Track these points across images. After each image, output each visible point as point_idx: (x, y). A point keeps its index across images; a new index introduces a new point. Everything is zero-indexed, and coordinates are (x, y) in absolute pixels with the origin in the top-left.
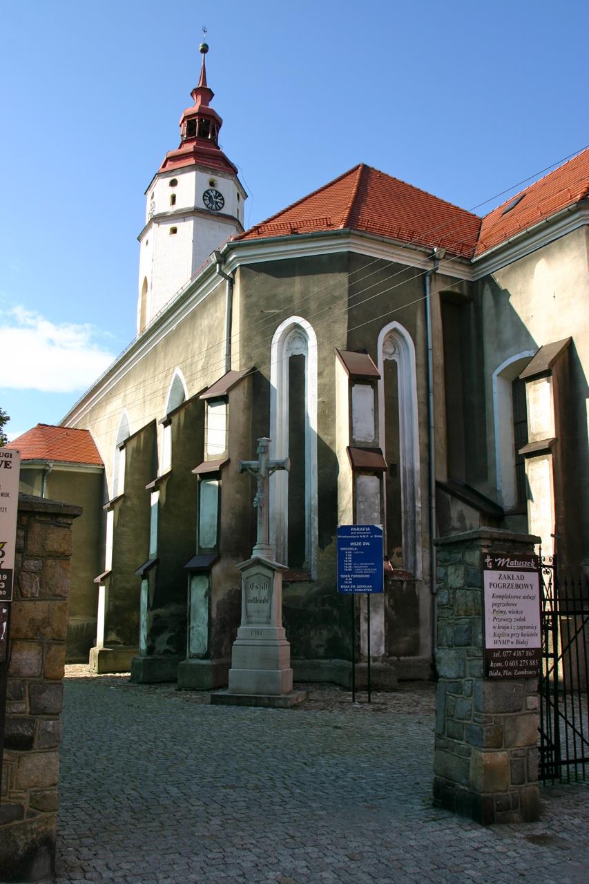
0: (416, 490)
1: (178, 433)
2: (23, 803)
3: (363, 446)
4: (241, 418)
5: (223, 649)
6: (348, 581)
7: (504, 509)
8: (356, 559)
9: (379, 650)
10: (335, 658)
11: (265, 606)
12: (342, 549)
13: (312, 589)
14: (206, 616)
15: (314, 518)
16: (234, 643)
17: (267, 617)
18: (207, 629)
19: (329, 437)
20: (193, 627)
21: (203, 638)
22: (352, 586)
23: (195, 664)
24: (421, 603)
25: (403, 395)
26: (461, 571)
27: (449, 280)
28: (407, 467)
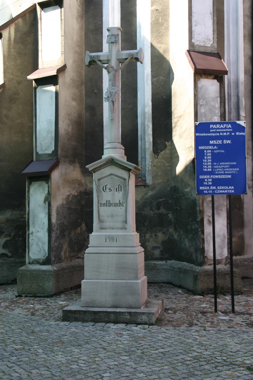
0: (240, 100)
1: (9, 48)
3: (202, 50)
4: (75, 25)
5: (62, 253)
6: (207, 182)
8: (216, 158)
9: (222, 252)
10: (170, 260)
11: (120, 210)
12: (200, 148)
13: (146, 194)
14: (46, 221)
15: (148, 125)
16: (86, 251)
17: (123, 222)
18: (47, 234)
19: (162, 46)
20: (32, 233)
21: (43, 244)
22: (211, 188)
23: (35, 270)
24: (245, 206)
25: (229, 8)
28: (232, 79)
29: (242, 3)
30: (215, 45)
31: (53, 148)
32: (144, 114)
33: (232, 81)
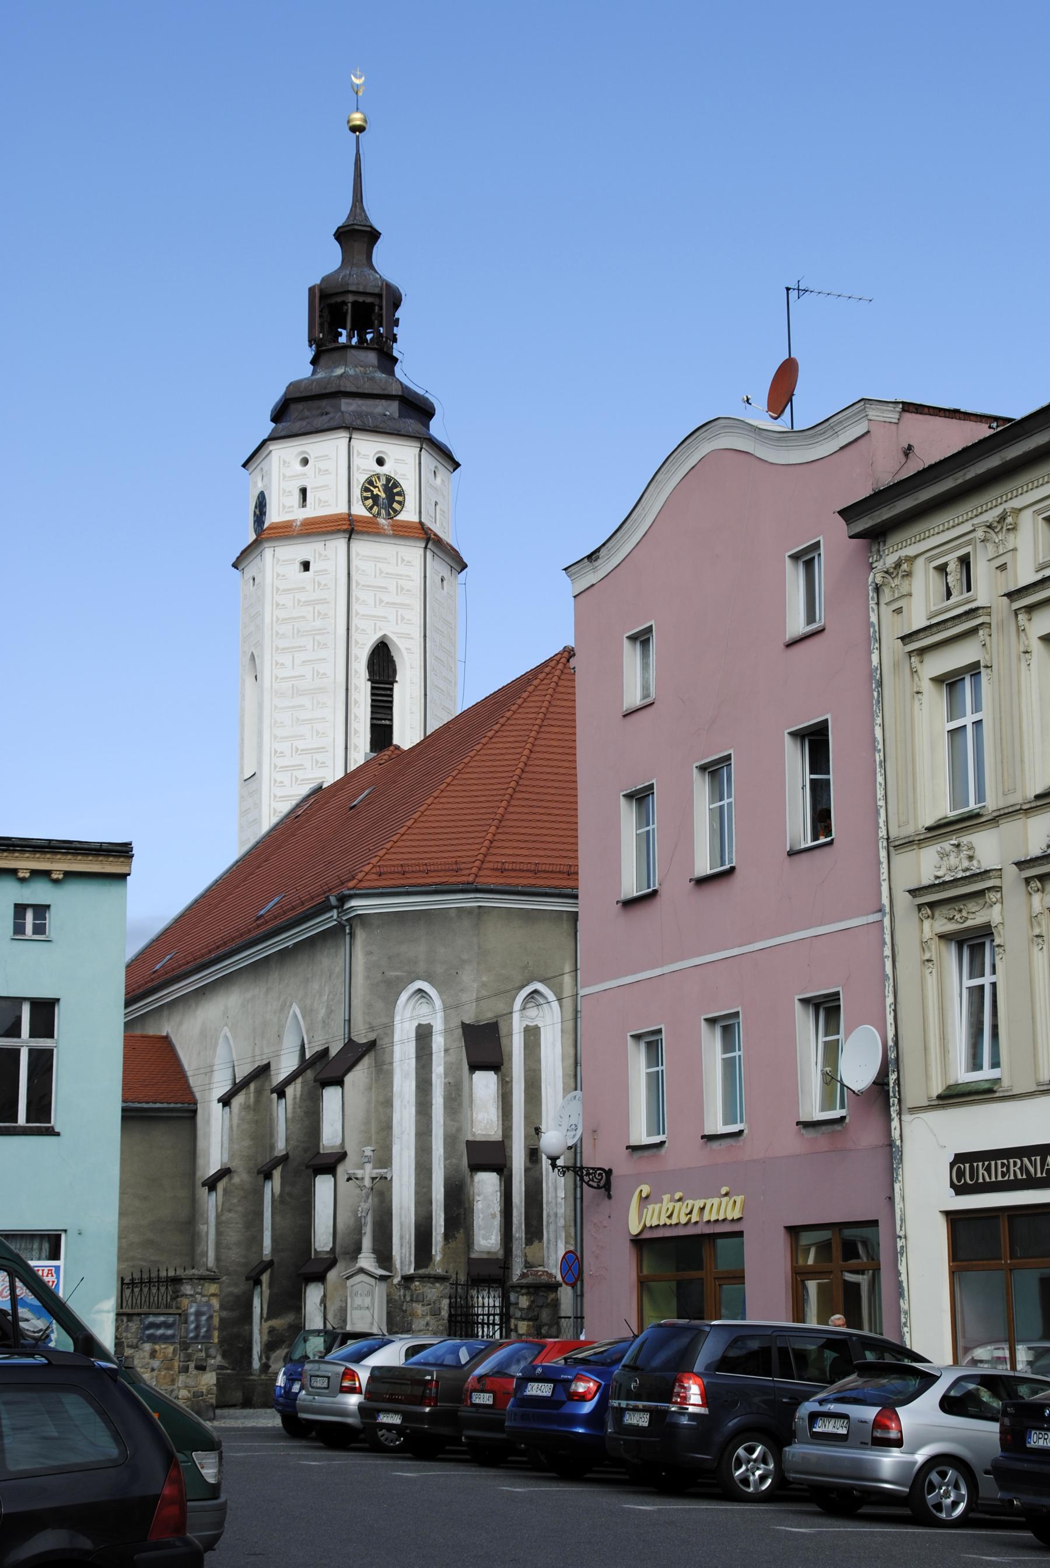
7: (493, 1250)
11: (367, 1313)
30: (500, 1133)
31: (331, 1245)
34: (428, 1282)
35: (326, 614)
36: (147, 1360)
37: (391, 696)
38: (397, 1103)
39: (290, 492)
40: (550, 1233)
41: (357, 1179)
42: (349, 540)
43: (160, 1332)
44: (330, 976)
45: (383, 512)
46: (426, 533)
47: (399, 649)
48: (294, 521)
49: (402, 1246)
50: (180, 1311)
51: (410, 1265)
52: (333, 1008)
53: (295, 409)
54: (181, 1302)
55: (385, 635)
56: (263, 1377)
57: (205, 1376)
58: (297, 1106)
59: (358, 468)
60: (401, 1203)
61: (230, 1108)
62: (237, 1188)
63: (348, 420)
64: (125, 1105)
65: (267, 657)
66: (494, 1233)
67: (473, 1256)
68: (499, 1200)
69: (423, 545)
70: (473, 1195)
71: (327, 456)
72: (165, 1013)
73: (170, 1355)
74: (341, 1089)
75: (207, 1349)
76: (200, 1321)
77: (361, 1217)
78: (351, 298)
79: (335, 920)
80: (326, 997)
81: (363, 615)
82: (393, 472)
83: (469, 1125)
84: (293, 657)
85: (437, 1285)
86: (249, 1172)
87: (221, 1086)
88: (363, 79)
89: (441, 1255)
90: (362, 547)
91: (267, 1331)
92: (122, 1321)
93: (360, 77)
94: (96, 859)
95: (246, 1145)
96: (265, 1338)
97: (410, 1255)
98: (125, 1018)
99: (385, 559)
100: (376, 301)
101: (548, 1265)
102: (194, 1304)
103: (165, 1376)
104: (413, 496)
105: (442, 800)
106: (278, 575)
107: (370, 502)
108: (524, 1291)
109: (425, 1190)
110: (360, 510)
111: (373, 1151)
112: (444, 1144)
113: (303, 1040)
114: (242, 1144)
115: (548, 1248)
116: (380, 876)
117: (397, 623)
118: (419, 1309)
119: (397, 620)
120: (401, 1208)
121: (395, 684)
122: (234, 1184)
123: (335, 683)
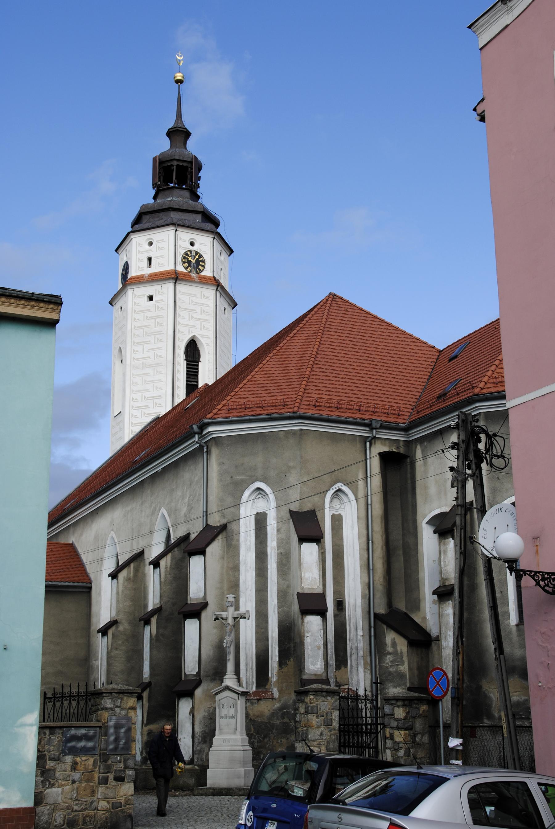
2: (121, 801)
7: (319, 673)
11: (233, 721)
15: (275, 648)
21: (189, 748)
26: (304, 706)
27: (387, 442)
29: (358, 540)
31: (197, 670)
32: (272, 638)
33: (351, 605)
34: (321, 696)
35: (162, 324)
36: (68, 772)
37: (198, 369)
38: (242, 568)
39: (142, 259)
40: (353, 661)
41: (222, 618)
42: (175, 284)
43: (82, 744)
44: (191, 484)
45: (193, 270)
46: (217, 282)
47: (202, 343)
48: (144, 275)
49: (247, 670)
50: (100, 724)
51: (253, 684)
52: (193, 506)
53: (145, 218)
54: (101, 715)
55: (194, 336)
56: (144, 767)
57: (123, 787)
58: (168, 573)
59: (180, 246)
60: (246, 640)
61: (117, 580)
62: (121, 634)
63: (175, 222)
64: (47, 583)
65: (128, 348)
66: (319, 660)
67: (305, 677)
68: (322, 636)
69: (215, 289)
70: (304, 633)
71: (163, 240)
72: (72, 530)
73: (91, 767)
74: (203, 557)
75: (125, 761)
76: (119, 733)
77: (226, 647)
78: (175, 163)
79: (197, 443)
80: (187, 499)
81: (182, 324)
82: (199, 249)
83: (299, 581)
84: (143, 347)
85: (329, 698)
86: (129, 623)
87: (110, 566)
88: (182, 57)
89: (277, 677)
90: (182, 288)
91: (146, 733)
92: (45, 734)
93: (181, 56)
94: (28, 303)
95: (128, 604)
96: (145, 738)
97: (253, 677)
98: (48, 536)
99: (195, 295)
100: (189, 165)
101: (352, 684)
102: (114, 717)
103: (85, 787)
104: (210, 263)
105: (264, 369)
106: (135, 303)
107: (186, 265)
108: (399, 703)
109: (263, 630)
110: (181, 268)
111: (235, 597)
112: (278, 597)
113: (169, 531)
114: (125, 604)
115: (351, 672)
116: (229, 411)
117: (201, 330)
118: (314, 720)
119: (201, 328)
120: (246, 644)
121: (200, 363)
122: (119, 631)
123: (167, 360)
